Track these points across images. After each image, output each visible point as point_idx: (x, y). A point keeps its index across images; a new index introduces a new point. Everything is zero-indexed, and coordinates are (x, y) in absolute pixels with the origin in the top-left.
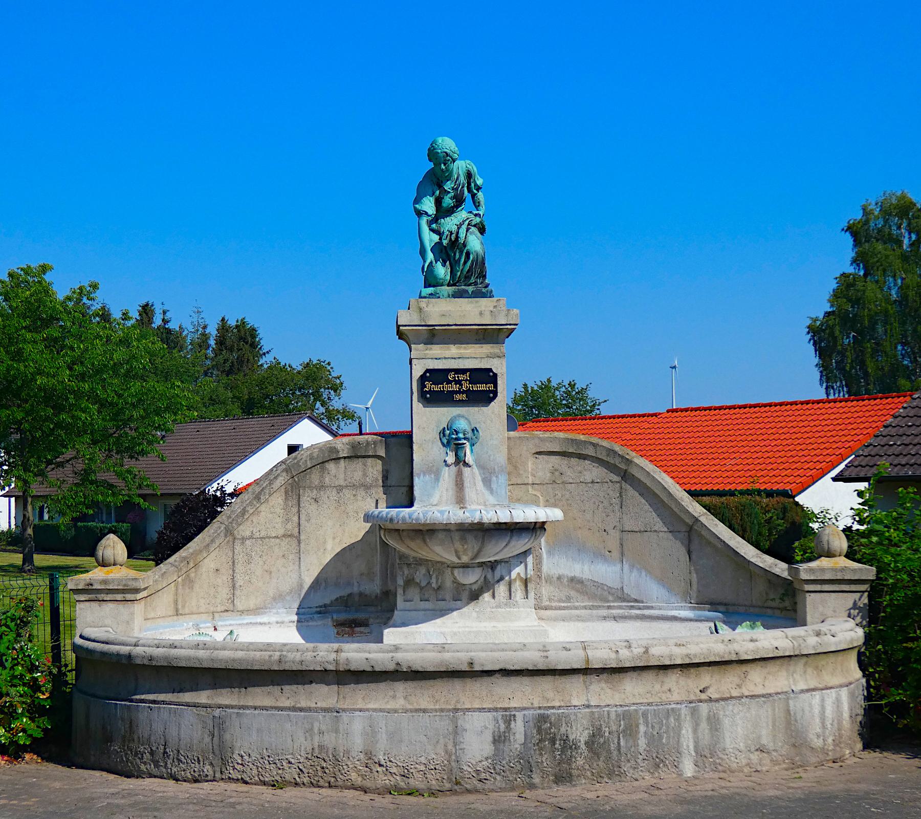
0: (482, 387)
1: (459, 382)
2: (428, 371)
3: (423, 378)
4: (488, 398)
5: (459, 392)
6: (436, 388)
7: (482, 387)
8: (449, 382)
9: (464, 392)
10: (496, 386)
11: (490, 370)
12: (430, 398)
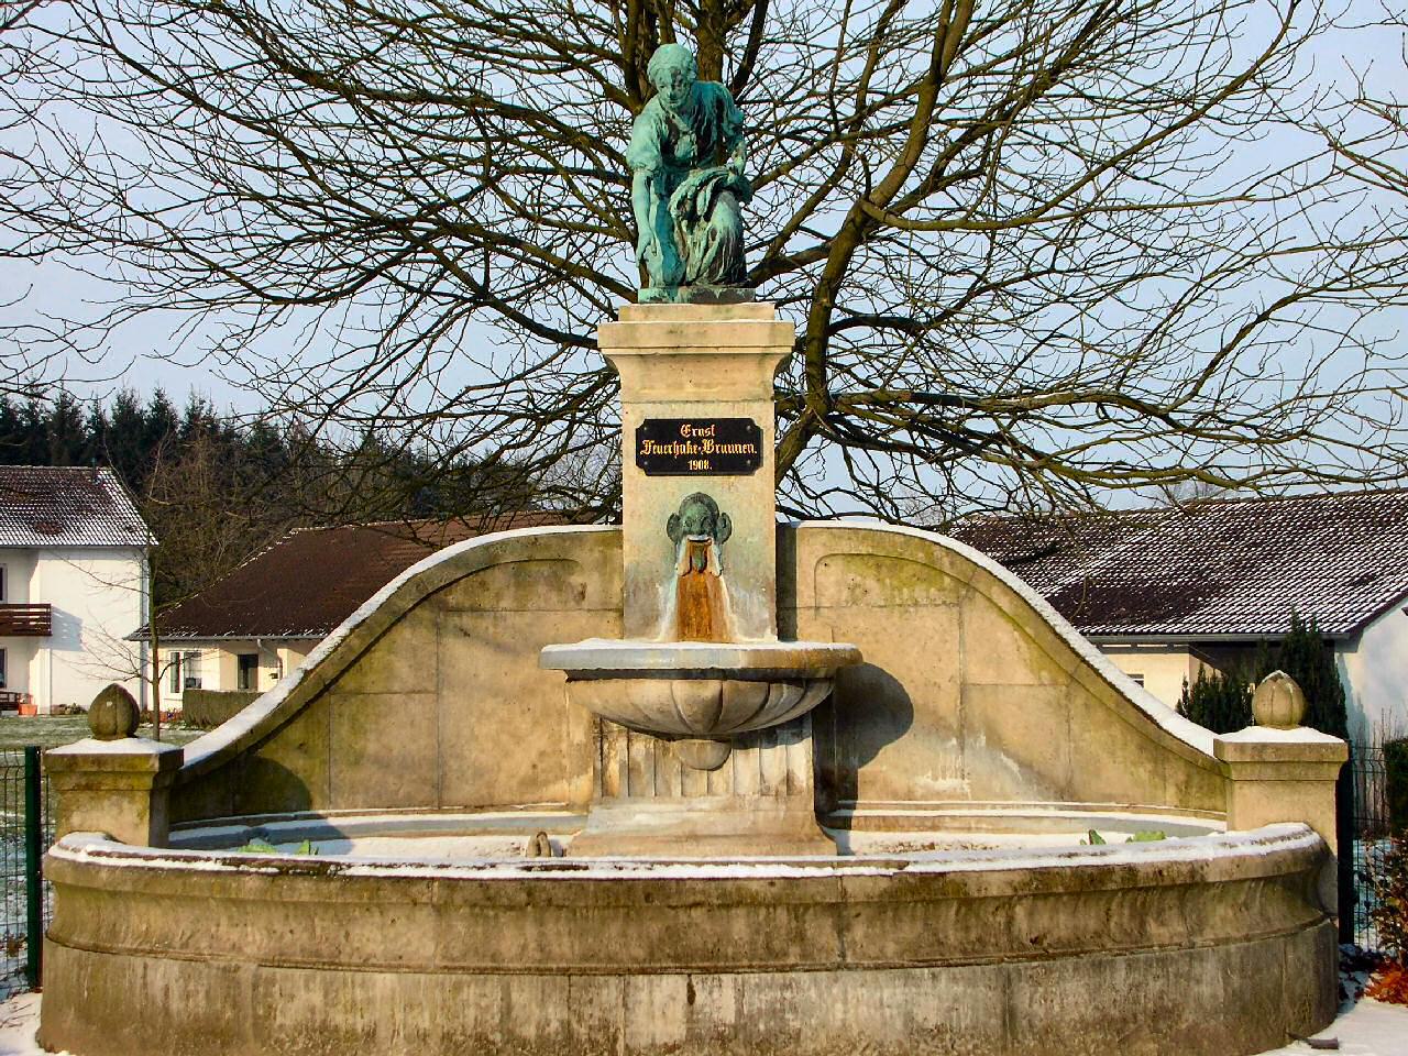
0: (740, 449)
1: (697, 441)
2: (647, 422)
3: (640, 435)
4: (744, 465)
5: (697, 457)
6: (659, 450)
7: (740, 449)
8: (682, 441)
9: (705, 456)
10: (759, 447)
11: (750, 421)
12: (654, 466)
